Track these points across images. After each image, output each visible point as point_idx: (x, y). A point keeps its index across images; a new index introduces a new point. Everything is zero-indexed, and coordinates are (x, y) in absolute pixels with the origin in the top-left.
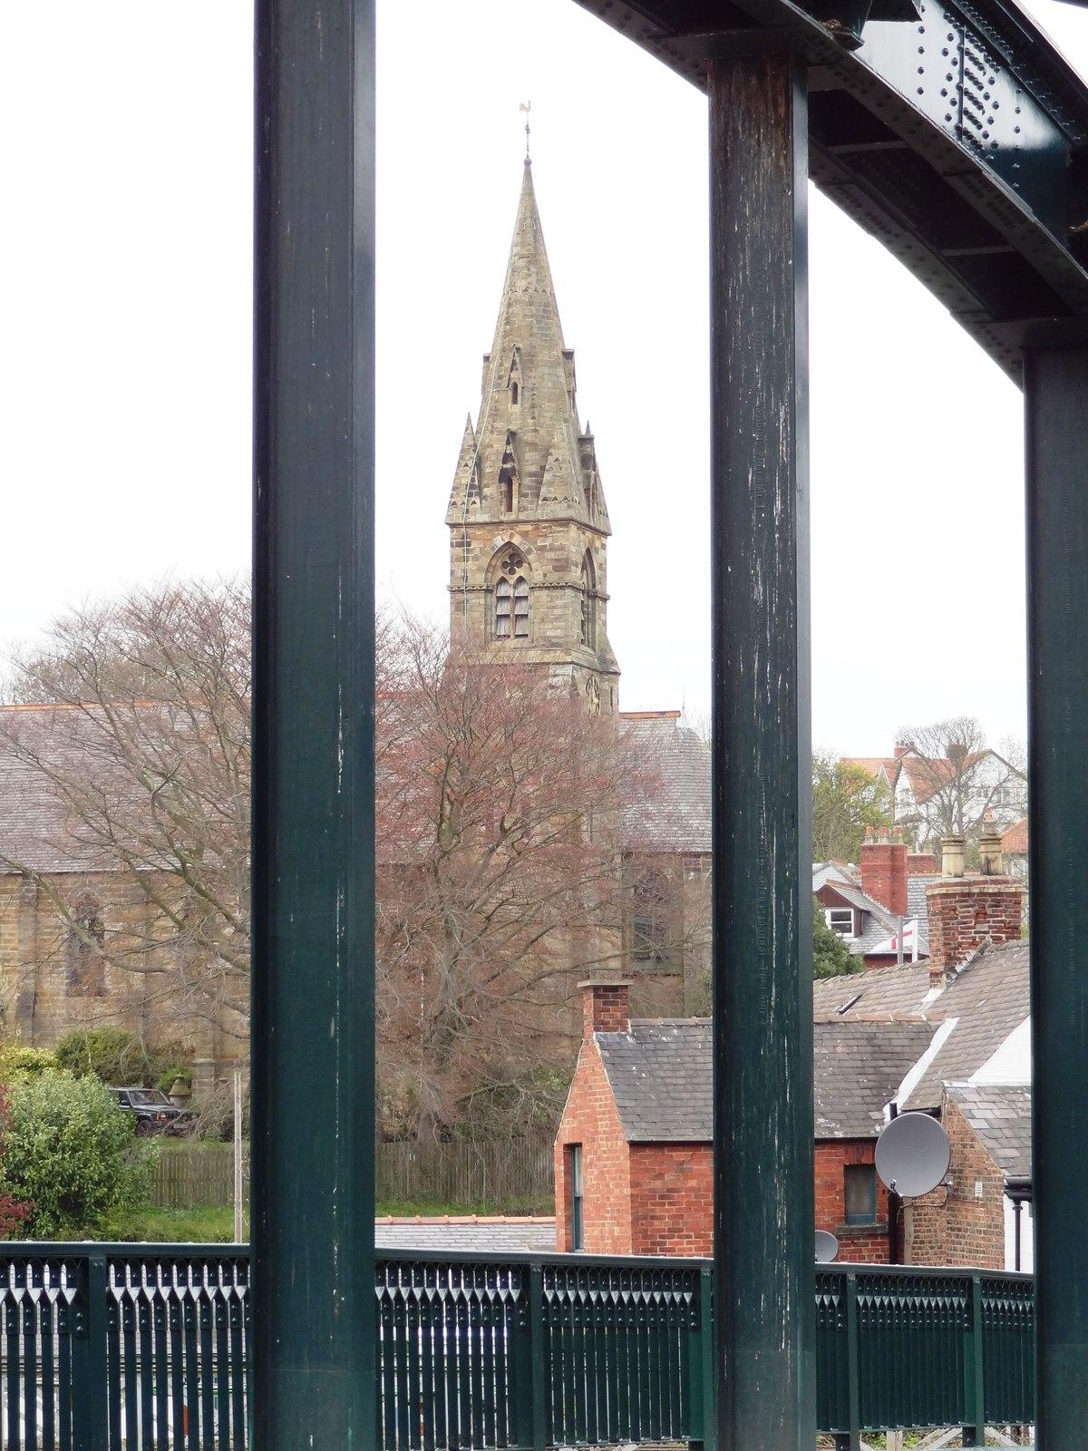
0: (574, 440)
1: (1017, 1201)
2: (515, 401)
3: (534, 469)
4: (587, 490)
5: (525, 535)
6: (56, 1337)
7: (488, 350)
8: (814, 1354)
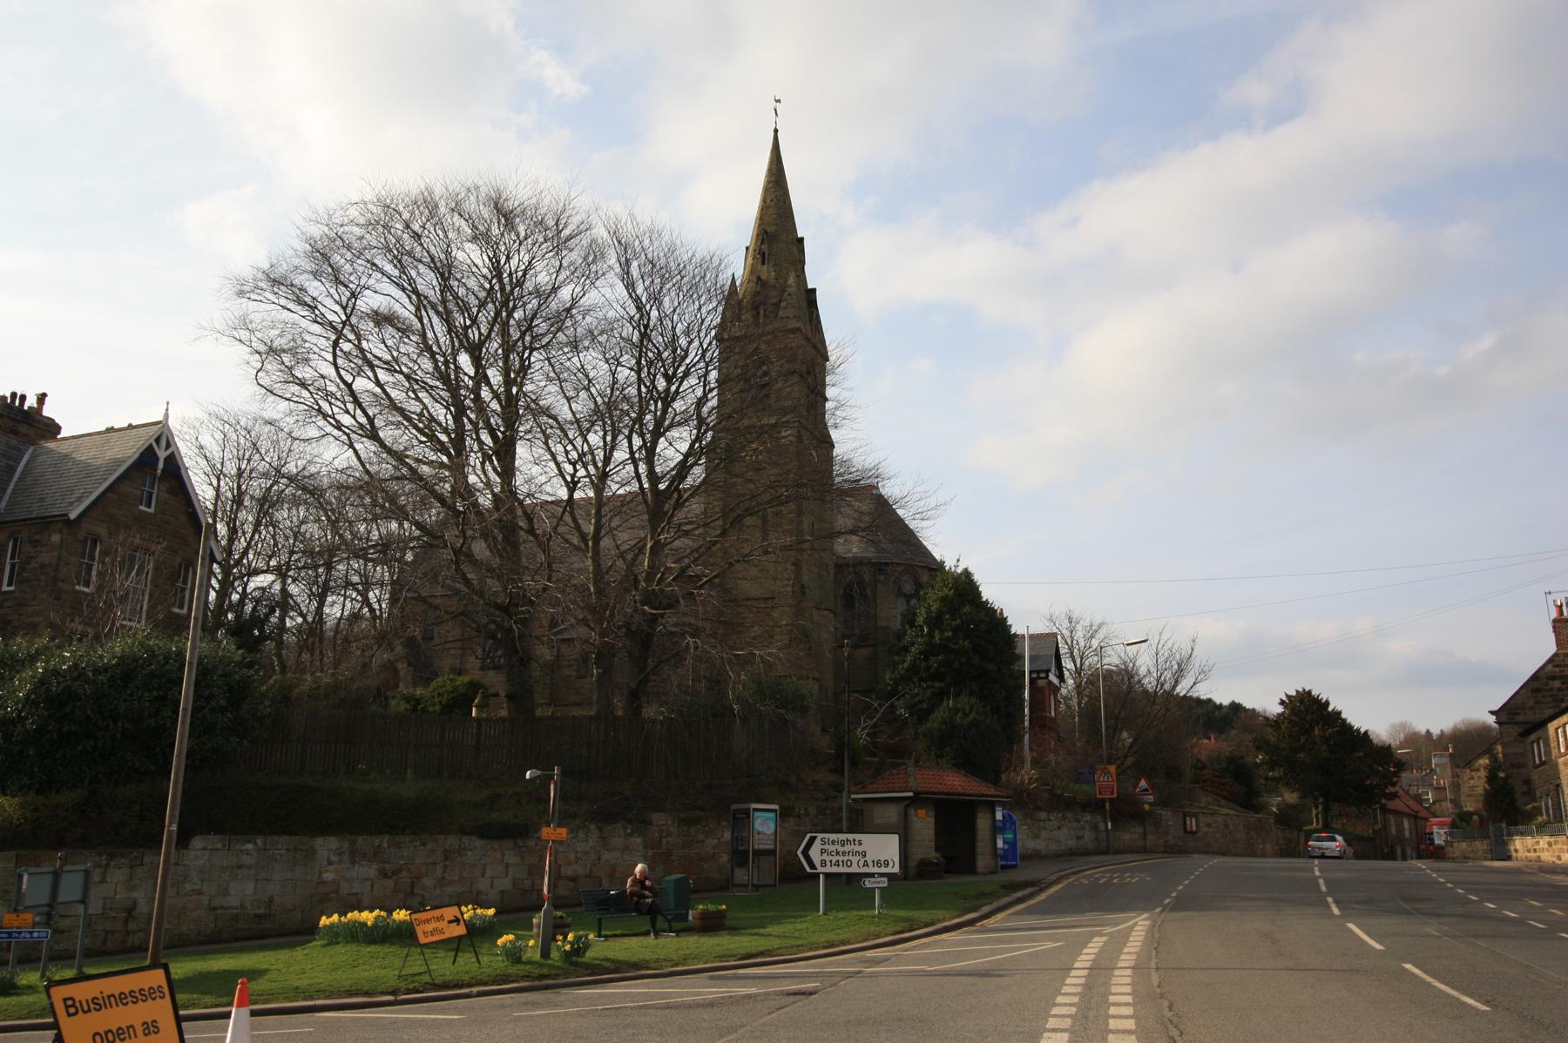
0: (803, 293)
1: (1055, 1005)
2: (763, 263)
3: (774, 301)
4: (811, 321)
5: (768, 342)
6: (570, 980)
7: (748, 244)
8: (933, 819)
